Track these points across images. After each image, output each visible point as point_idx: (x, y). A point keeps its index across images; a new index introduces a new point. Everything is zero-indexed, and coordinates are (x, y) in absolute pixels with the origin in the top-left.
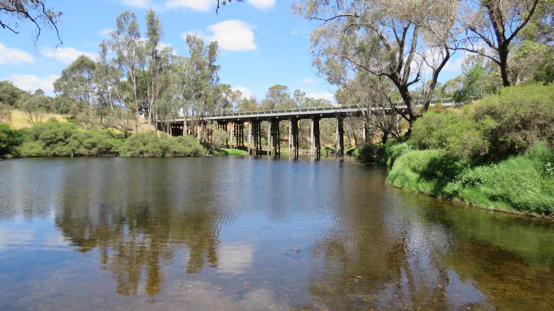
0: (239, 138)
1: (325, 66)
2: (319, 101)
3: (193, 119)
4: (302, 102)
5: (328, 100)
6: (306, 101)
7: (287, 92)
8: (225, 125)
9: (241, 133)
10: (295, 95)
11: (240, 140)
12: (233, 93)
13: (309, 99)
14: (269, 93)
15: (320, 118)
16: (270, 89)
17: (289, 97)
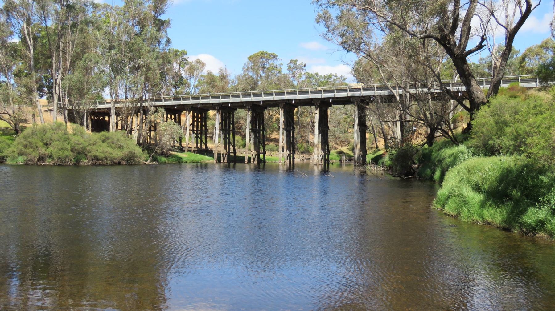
0: (199, 136)
1: (336, 22)
5: (341, 77)
6: (307, 78)
7: (277, 63)
10: (290, 68)
11: (201, 139)
12: (191, 63)
13: (312, 75)
16: (251, 58)
17: (280, 72)
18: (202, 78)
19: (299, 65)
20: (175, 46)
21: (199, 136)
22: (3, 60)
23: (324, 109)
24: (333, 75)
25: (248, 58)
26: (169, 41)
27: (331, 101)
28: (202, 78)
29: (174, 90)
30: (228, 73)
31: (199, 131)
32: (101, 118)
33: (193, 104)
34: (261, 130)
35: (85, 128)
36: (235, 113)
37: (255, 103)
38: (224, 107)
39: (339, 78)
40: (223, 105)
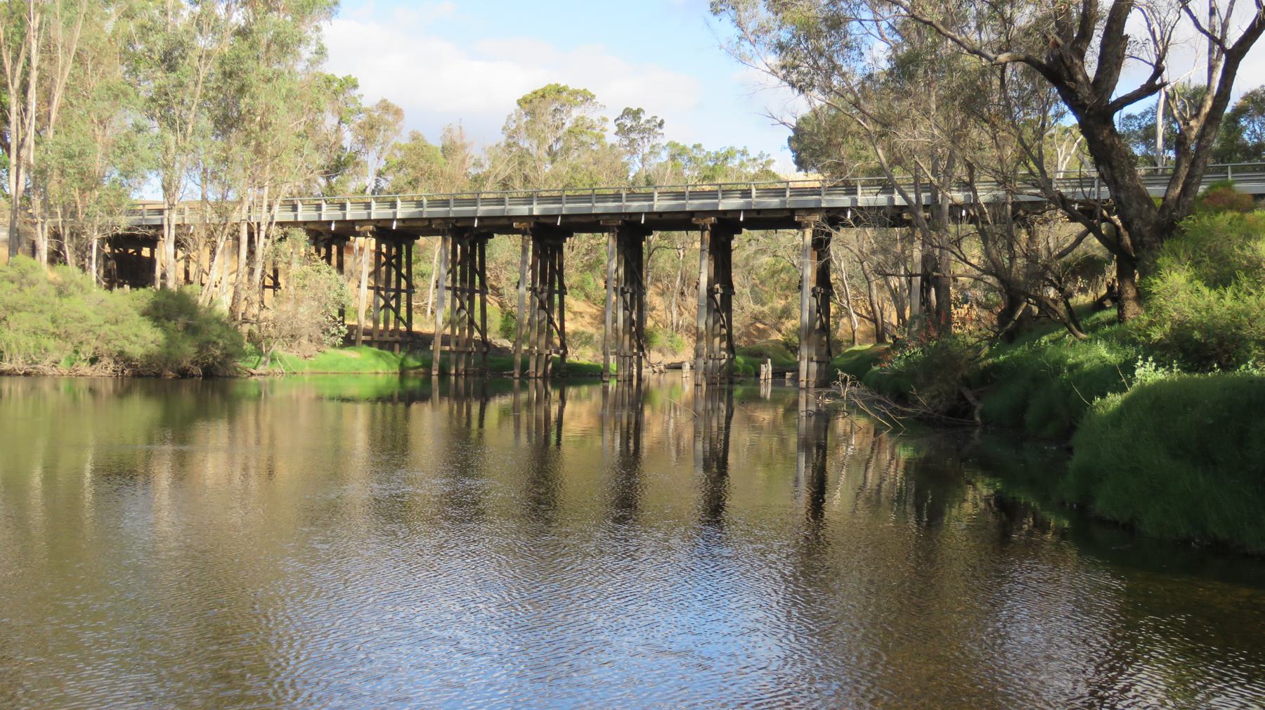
0: (393, 303)
2: (726, 159)
3: (203, 217)
4: (654, 162)
5: (761, 156)
6: (673, 158)
7: (592, 115)
8: (334, 249)
9: (404, 284)
10: (622, 131)
11: (397, 310)
13: (684, 148)
14: (519, 118)
15: (648, 230)
16: (523, 102)
17: (599, 138)
18: (396, 152)
19: (648, 121)
20: (335, 68)
21: (393, 303)
22: (803, 6)
23: (723, 239)
24: (739, 151)
25: (519, 103)
26: (321, 52)
27: (741, 219)
28: (396, 152)
29: (323, 182)
30: (466, 140)
31: (393, 290)
32: (131, 251)
33: (458, 219)
34: (556, 292)
35: (72, 268)
36: (487, 248)
37: (542, 220)
38: (460, 228)
39: (755, 160)
40: (459, 225)
